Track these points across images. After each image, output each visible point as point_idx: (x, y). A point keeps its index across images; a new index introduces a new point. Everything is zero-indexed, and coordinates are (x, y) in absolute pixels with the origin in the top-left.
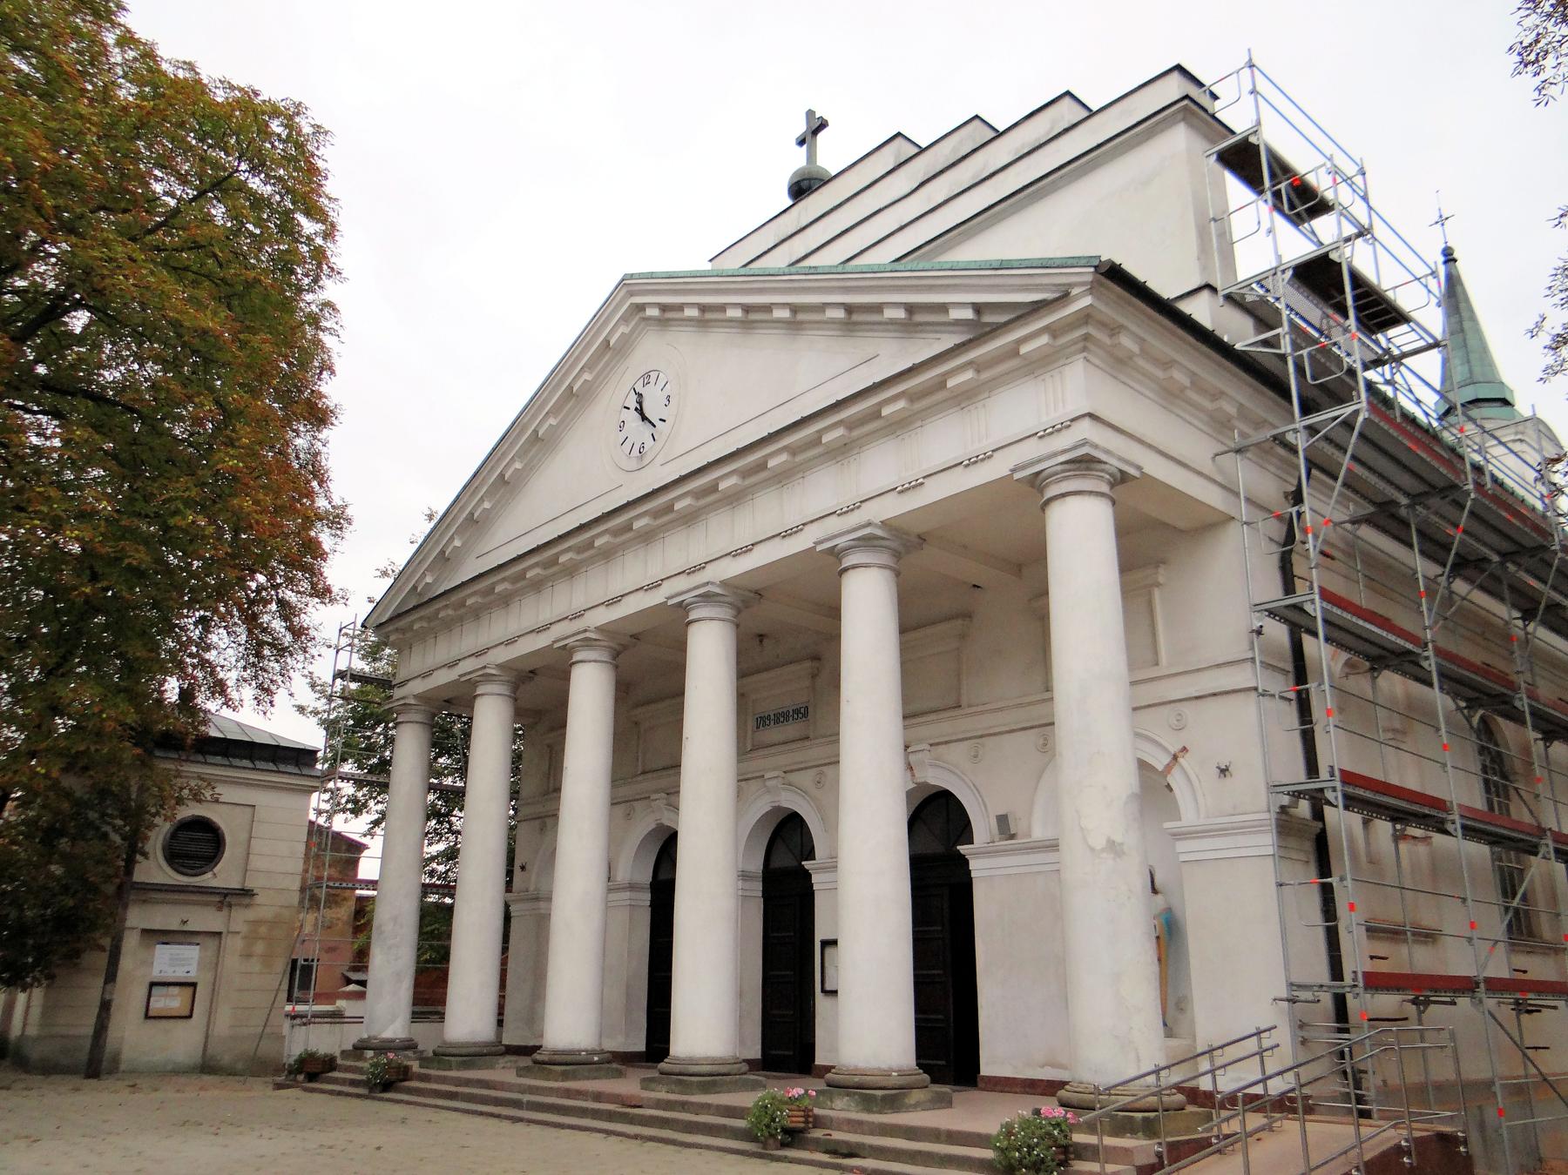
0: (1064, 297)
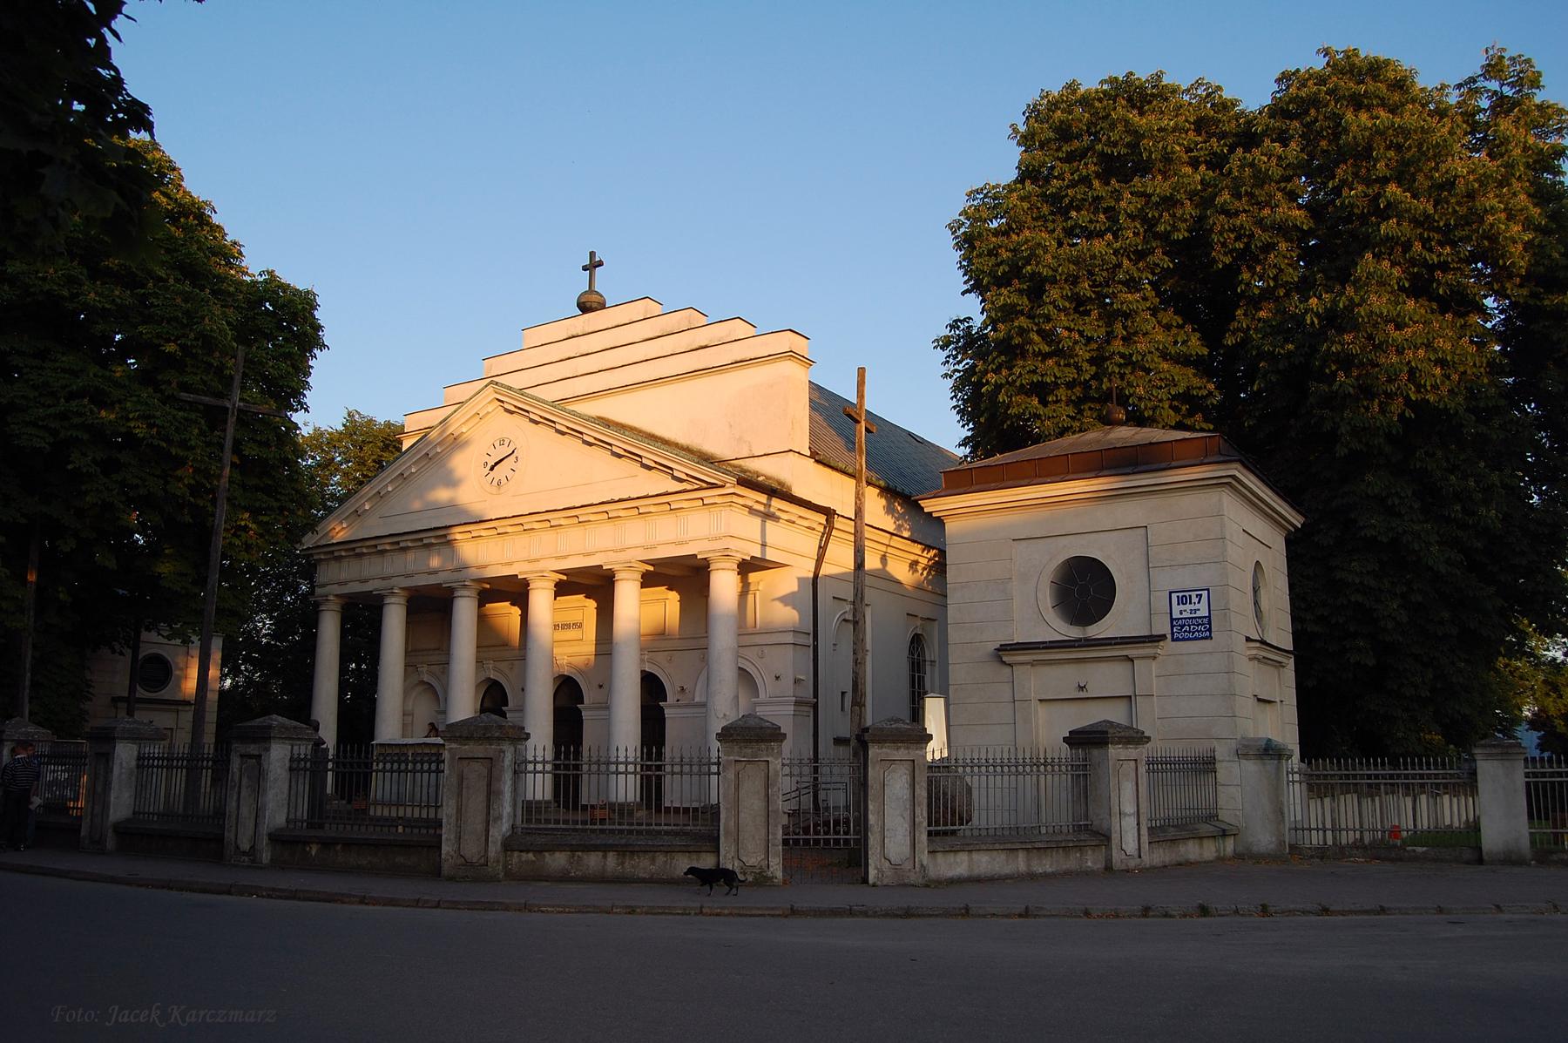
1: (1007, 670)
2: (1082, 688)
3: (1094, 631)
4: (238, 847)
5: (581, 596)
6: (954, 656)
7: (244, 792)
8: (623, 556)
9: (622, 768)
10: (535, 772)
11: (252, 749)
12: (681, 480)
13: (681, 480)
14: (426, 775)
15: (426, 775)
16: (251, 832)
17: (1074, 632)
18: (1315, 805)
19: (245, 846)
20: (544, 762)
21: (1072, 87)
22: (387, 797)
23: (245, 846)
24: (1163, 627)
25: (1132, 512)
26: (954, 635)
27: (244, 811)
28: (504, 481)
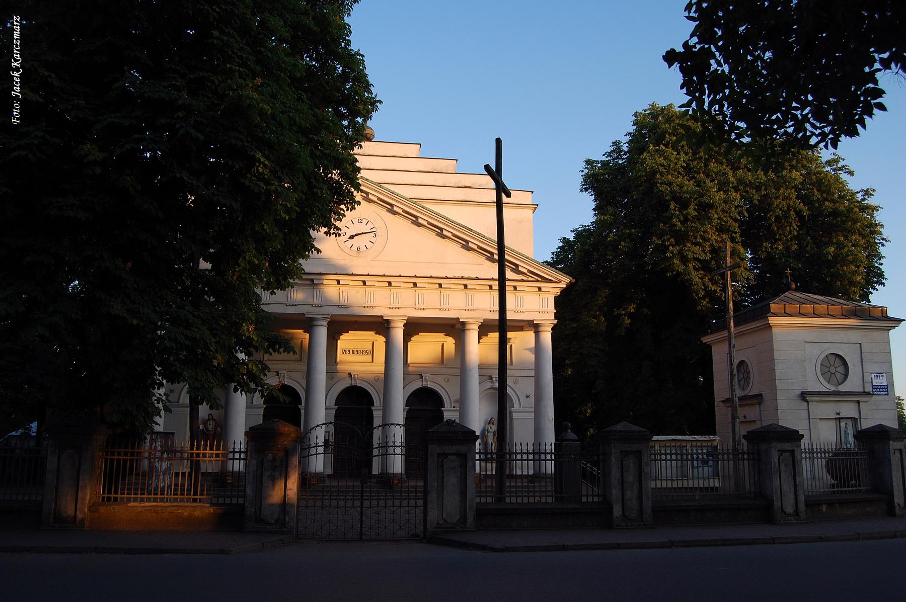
0: (560, 282)
1: (805, 404)
2: (838, 414)
3: (843, 388)
4: (783, 511)
5: (372, 333)
6: (780, 396)
7: (783, 475)
8: (473, 314)
9: (519, 457)
10: (522, 460)
11: (787, 446)
12: (523, 273)
13: (523, 273)
14: (663, 463)
15: (663, 463)
16: (792, 500)
17: (832, 388)
18: (820, 464)
19: (790, 509)
20: (528, 453)
21: (653, 106)
22: (669, 474)
23: (790, 509)
24: (868, 389)
25: (855, 336)
26: (779, 385)
27: (785, 487)
28: (363, 248)
